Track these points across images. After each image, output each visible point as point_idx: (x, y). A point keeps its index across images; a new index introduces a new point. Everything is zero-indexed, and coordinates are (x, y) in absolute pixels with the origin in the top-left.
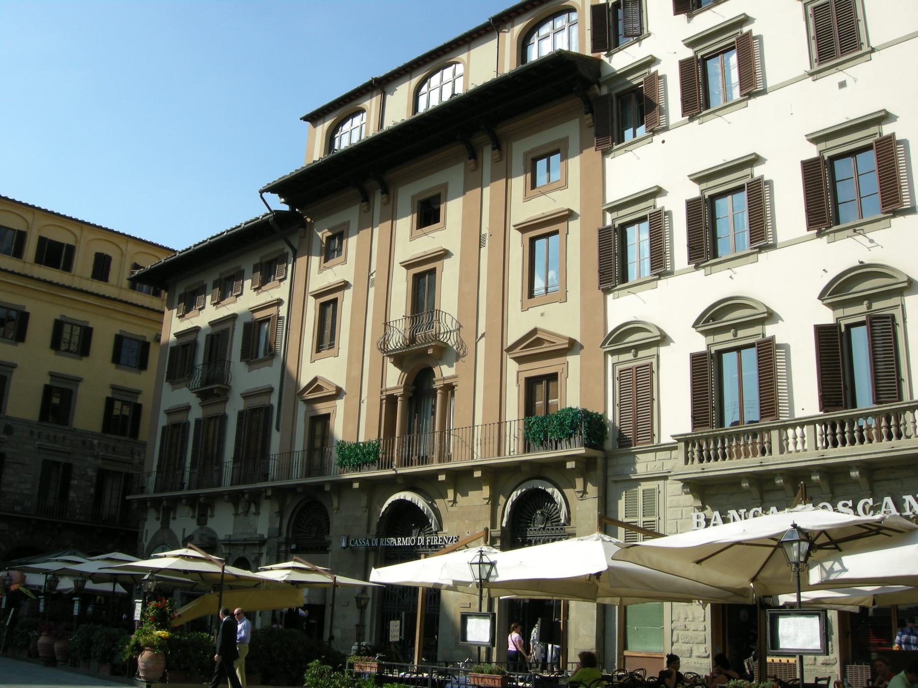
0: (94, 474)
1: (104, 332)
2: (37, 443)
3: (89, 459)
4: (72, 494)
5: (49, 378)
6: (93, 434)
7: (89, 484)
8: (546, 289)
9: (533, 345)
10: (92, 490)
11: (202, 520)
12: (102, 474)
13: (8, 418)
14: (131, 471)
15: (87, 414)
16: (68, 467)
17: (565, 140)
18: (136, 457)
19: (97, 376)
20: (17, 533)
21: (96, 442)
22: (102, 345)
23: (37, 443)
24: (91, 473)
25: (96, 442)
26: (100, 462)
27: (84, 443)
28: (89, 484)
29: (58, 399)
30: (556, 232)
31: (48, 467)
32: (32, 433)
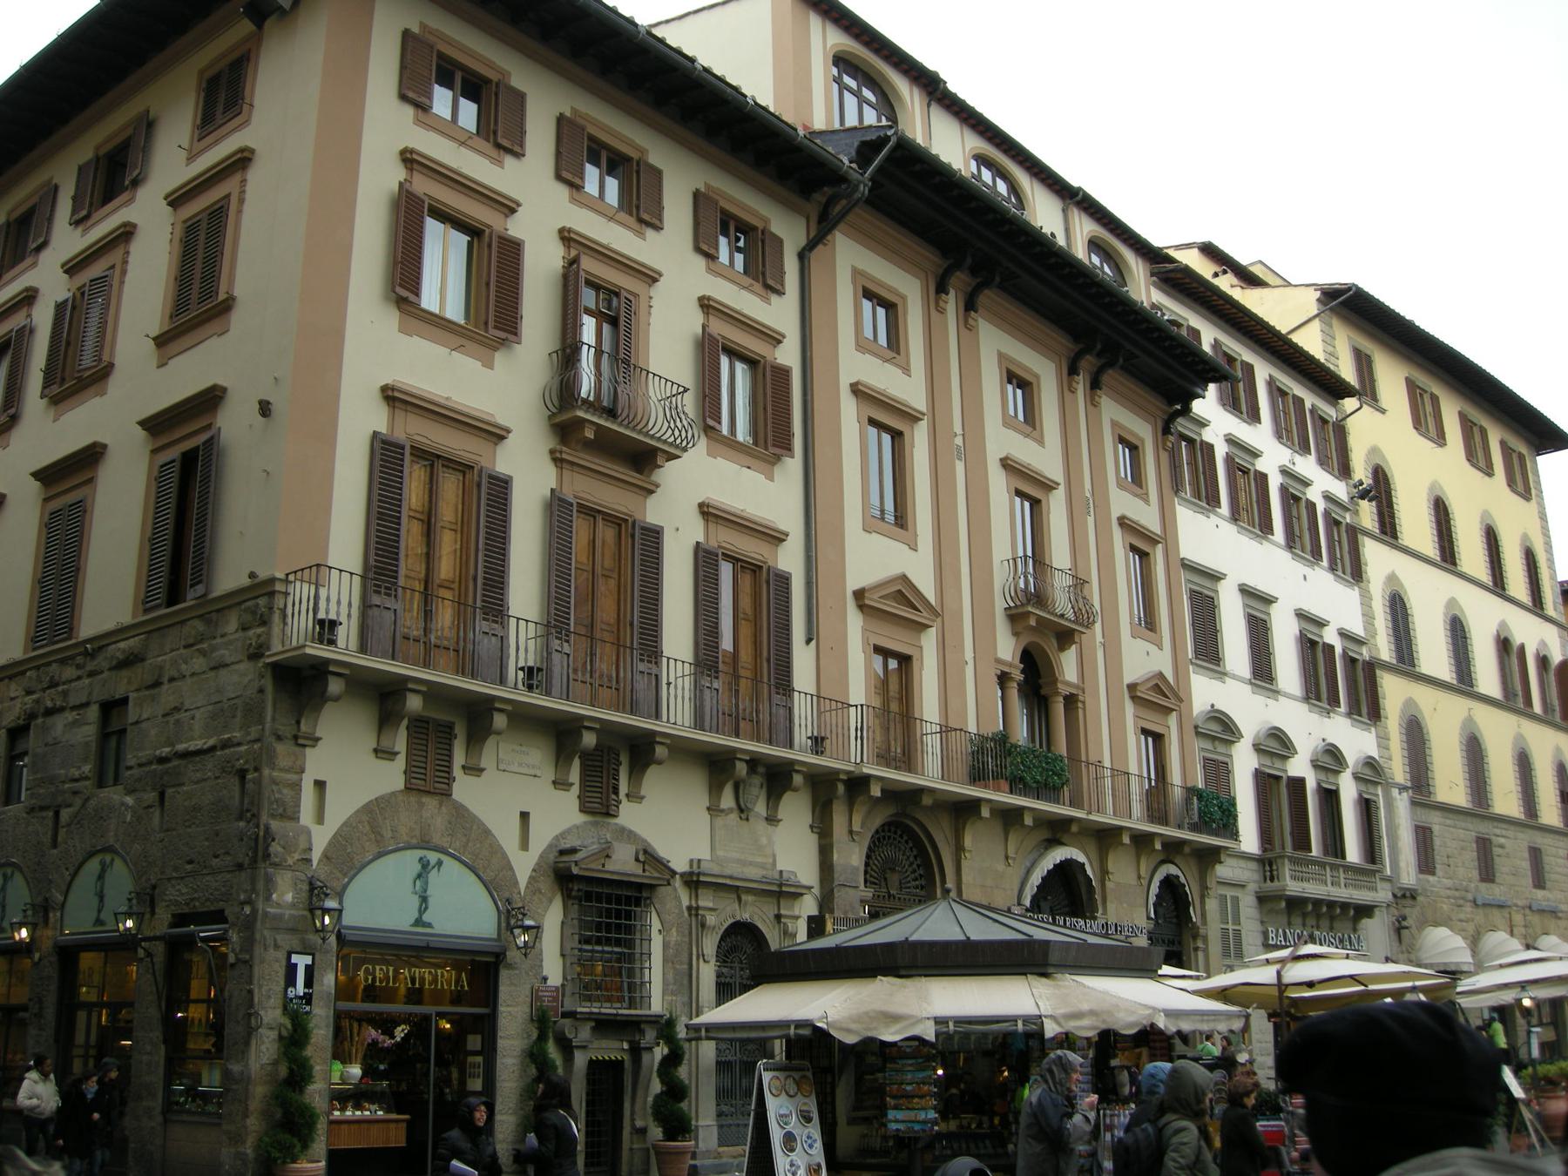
11: (428, 777)
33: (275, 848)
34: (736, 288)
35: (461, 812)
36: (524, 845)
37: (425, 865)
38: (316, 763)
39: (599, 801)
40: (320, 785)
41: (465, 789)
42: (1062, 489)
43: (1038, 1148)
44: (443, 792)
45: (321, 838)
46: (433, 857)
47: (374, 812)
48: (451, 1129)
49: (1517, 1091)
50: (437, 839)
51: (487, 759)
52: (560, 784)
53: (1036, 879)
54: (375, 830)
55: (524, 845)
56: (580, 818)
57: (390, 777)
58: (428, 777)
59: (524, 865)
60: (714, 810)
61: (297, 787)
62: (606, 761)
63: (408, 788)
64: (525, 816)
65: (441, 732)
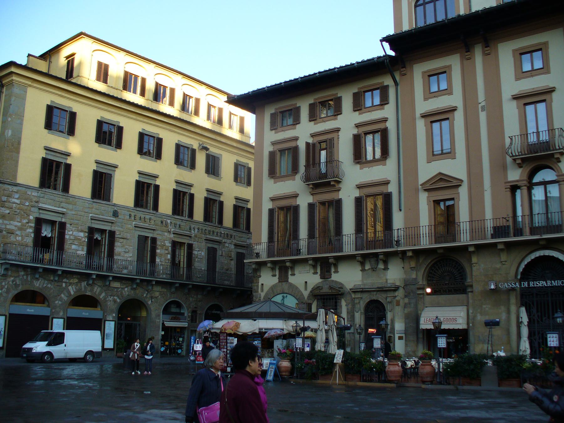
0: (170, 245)
1: (132, 129)
2: (134, 223)
3: (166, 234)
4: (158, 260)
5: (138, 175)
6: (167, 216)
7: (167, 252)
8: (442, 150)
9: (443, 184)
10: (169, 256)
11: (283, 278)
12: (175, 244)
13: (115, 205)
14: (63, 220)
15: (123, 193)
16: (154, 240)
17: (450, 67)
18: (193, 232)
19: (128, 166)
20: (126, 289)
21: (169, 221)
22: (130, 140)
23: (134, 223)
24: (168, 244)
25: (169, 221)
26: (172, 236)
27: (162, 222)
28: (167, 252)
29: (54, 172)
30: (448, 119)
31: (142, 240)
32: (130, 216)
33: (254, 298)
34: (33, 68)
35: (291, 285)
36: (306, 289)
37: (283, 297)
38: (261, 281)
39: (325, 275)
40: (262, 284)
41: (291, 279)
42: (418, 115)
43: (412, 379)
44: (286, 280)
45: (263, 295)
46: (285, 295)
47: (273, 288)
48: (542, 364)
49: (357, 409)
50: (285, 292)
51: (296, 272)
52: (315, 273)
53: (523, 266)
54: (273, 291)
55: (306, 289)
56: (321, 280)
57: (276, 280)
58: (283, 278)
59: (306, 294)
60: (363, 270)
61: (258, 286)
62: (325, 266)
63: (279, 282)
64: (306, 282)
65: (283, 269)
